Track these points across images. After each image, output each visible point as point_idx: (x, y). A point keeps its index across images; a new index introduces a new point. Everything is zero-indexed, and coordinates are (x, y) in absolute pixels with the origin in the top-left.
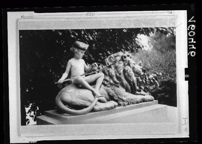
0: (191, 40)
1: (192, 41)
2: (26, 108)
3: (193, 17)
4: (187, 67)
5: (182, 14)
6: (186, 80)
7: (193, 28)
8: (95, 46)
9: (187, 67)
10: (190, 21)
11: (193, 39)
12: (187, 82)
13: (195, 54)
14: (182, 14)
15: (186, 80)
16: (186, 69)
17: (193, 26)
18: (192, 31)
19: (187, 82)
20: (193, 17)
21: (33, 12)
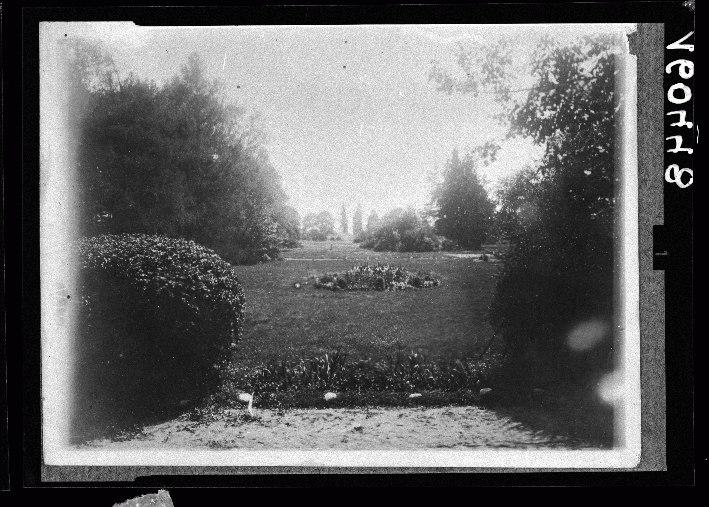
0: (677, 118)
1: (682, 123)
2: (632, 27)
3: (691, 33)
4: (661, 222)
5: (56, 38)
6: (656, 267)
7: (687, 70)
8: (232, 265)
9: (661, 222)
10: (675, 46)
11: (683, 114)
12: (661, 273)
13: (691, 73)
14: (56, 38)
15: (656, 267)
16: (656, 228)
17: (684, 63)
18: (686, 82)
19: (661, 273)
20: (691, 33)
21: (160, 85)
